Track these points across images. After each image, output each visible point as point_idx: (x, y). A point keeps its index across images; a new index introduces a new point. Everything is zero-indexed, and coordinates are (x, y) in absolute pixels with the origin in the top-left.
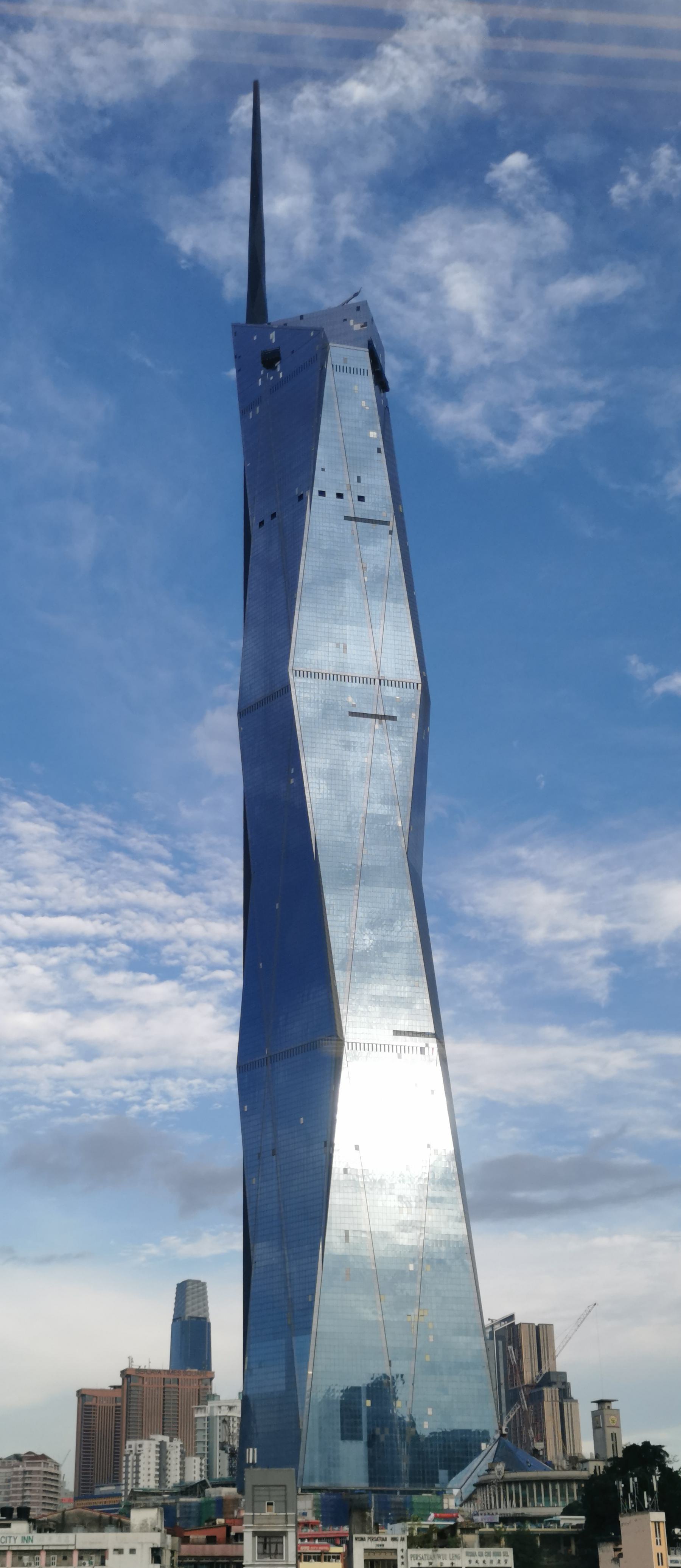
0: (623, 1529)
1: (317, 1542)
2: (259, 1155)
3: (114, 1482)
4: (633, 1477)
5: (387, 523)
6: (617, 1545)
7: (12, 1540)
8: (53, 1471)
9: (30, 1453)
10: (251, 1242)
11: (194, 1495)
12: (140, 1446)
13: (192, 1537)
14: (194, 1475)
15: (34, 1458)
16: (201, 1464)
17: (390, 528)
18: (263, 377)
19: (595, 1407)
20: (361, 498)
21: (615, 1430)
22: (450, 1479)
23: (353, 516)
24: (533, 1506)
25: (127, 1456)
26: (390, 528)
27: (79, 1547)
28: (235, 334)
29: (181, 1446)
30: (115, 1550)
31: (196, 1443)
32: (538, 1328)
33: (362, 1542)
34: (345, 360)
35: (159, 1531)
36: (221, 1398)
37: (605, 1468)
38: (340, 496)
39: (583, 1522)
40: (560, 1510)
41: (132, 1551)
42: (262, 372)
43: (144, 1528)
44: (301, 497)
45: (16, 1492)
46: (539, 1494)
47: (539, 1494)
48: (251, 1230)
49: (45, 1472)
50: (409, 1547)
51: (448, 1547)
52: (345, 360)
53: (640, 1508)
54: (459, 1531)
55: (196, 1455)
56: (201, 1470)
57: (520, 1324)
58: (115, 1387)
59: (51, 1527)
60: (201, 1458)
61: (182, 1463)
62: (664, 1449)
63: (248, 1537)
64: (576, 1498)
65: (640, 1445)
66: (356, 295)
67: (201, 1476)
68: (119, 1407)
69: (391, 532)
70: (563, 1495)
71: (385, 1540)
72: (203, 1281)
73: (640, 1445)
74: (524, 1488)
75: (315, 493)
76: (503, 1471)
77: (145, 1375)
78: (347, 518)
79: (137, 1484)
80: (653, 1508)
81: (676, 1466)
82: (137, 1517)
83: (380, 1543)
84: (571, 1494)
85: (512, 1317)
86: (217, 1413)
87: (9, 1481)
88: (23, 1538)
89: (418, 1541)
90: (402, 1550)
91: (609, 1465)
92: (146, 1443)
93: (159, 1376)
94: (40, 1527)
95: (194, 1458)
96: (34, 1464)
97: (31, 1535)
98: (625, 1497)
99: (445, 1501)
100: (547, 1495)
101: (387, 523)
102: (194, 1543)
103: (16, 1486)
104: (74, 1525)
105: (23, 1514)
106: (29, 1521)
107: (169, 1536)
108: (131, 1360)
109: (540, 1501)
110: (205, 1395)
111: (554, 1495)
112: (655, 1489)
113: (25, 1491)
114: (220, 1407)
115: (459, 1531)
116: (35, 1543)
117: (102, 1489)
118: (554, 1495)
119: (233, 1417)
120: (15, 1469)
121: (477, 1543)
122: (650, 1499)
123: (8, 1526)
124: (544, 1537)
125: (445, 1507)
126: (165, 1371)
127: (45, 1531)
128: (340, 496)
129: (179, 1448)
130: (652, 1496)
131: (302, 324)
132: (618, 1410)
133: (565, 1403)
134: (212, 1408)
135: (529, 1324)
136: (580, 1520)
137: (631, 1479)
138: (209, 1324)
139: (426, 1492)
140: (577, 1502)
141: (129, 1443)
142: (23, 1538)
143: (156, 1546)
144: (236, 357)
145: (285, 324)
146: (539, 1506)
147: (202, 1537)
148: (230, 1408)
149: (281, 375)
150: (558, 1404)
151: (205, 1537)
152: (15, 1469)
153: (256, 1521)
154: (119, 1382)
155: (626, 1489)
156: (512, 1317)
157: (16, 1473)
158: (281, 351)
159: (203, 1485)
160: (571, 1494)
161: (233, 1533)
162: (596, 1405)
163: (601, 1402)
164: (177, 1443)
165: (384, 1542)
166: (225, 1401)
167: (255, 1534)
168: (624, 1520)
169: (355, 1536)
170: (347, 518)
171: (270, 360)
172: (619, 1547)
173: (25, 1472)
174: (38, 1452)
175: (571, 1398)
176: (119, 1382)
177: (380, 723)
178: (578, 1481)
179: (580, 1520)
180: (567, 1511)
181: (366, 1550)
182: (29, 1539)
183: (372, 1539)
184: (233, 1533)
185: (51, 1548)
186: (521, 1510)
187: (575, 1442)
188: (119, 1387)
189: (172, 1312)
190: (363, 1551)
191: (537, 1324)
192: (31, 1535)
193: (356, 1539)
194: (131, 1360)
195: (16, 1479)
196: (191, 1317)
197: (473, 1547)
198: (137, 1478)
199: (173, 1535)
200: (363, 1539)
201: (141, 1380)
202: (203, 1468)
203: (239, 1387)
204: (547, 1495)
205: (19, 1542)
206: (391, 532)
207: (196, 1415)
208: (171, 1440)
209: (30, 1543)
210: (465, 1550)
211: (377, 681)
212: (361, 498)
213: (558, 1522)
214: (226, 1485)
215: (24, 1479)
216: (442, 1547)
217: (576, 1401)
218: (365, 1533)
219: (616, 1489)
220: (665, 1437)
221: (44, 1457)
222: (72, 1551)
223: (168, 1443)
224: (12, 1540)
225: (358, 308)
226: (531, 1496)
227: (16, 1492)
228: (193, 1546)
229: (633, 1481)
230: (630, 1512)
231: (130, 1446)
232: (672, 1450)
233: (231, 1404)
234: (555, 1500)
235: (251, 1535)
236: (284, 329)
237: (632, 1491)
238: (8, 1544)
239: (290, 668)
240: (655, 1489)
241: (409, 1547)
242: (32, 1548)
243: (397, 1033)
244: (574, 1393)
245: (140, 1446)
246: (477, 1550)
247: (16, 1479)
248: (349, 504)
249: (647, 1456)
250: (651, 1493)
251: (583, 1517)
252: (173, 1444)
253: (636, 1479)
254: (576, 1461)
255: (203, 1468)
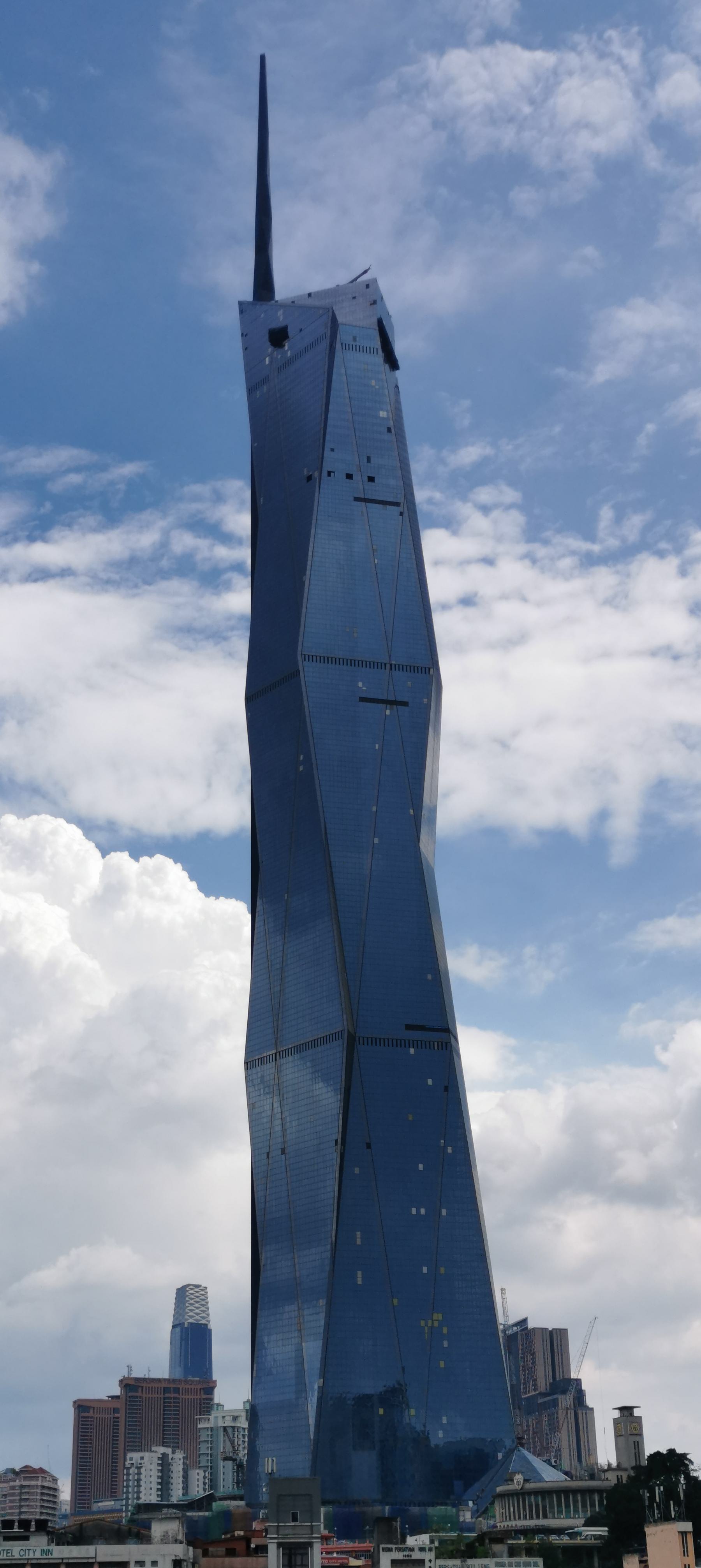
0: (649, 1540)
1: (335, 1555)
2: (268, 1154)
3: (112, 1496)
4: (659, 1486)
5: (397, 504)
6: (643, 1556)
7: (31, 1552)
8: (51, 1485)
9: (26, 1467)
10: (260, 1244)
11: (200, 1509)
12: (142, 1458)
13: (211, 1549)
14: (198, 1491)
15: (28, 1472)
16: (205, 1477)
17: (401, 509)
18: (271, 355)
19: (617, 1414)
20: (371, 479)
21: (637, 1439)
22: (465, 1490)
23: (362, 497)
24: (554, 1518)
25: (128, 1469)
26: (401, 509)
27: (99, 1559)
28: (241, 312)
29: (184, 1458)
30: (136, 1562)
31: (200, 1455)
32: (551, 1332)
33: (389, 1553)
34: (355, 339)
35: (181, 1543)
36: (225, 1408)
37: (629, 1477)
38: (349, 476)
39: (606, 1534)
40: (582, 1521)
41: (154, 1563)
42: (270, 350)
43: (165, 1540)
44: (309, 478)
45: (11, 1508)
46: (559, 1505)
47: (559, 1505)
48: (259, 1232)
49: (43, 1487)
50: (437, 1557)
51: (476, 1558)
52: (355, 339)
53: (666, 1518)
54: (487, 1541)
55: (200, 1467)
56: (205, 1484)
57: (534, 1329)
58: (113, 1397)
59: (69, 1540)
60: (205, 1471)
61: (186, 1477)
62: (688, 1457)
63: (272, 1549)
64: (597, 1509)
65: (665, 1452)
66: (365, 272)
67: (205, 1490)
68: (118, 1418)
69: (402, 514)
70: (584, 1506)
71: (412, 1550)
72: (203, 1285)
73: (665, 1452)
74: (543, 1499)
75: (325, 473)
76: (522, 1481)
77: (144, 1385)
78: (357, 499)
79: (138, 1498)
80: (680, 1518)
81: (698, 1474)
82: (157, 1529)
83: (407, 1553)
84: (593, 1505)
85: (525, 1321)
86: (221, 1424)
87: (5, 1496)
88: (43, 1551)
89: (444, 1551)
90: (430, 1561)
91: (632, 1473)
92: (146, 1455)
93: (159, 1385)
94: (60, 1538)
95: (197, 1471)
96: (31, 1478)
97: (50, 1548)
98: (651, 1507)
99: (461, 1513)
100: (567, 1506)
101: (397, 504)
102: (213, 1556)
103: (11, 1501)
104: (94, 1537)
105: (42, 1526)
106: (48, 1533)
107: (191, 1548)
108: (130, 1368)
109: (560, 1512)
110: (206, 1405)
111: (575, 1506)
112: (682, 1498)
113: (21, 1506)
114: (224, 1417)
115: (487, 1541)
116: (55, 1555)
117: (100, 1504)
118: (575, 1506)
119: (238, 1428)
120: (12, 1484)
121: (506, 1554)
122: (677, 1509)
123: (26, 1538)
124: (566, 1549)
125: (461, 1519)
126: (165, 1380)
127: (63, 1545)
128: (349, 476)
129: (182, 1461)
130: (679, 1507)
131: (309, 302)
132: (640, 1417)
133: (580, 1412)
134: (216, 1418)
135: (542, 1329)
136: (602, 1531)
137: (657, 1488)
138: (210, 1330)
139: (442, 1504)
140: (599, 1513)
141: (129, 1455)
142: (43, 1551)
143: (178, 1558)
144: (242, 335)
145: (293, 302)
146: (559, 1518)
147: (222, 1550)
148: (235, 1418)
149: (289, 354)
150: (573, 1412)
151: (224, 1549)
152: (12, 1484)
153: (281, 1532)
154: (117, 1391)
155: (652, 1498)
156: (525, 1321)
157: (13, 1488)
158: (289, 330)
159: (210, 1499)
160: (593, 1505)
161: (253, 1546)
162: (618, 1412)
163: (622, 1409)
164: (179, 1455)
165: (411, 1553)
166: (231, 1411)
167: (279, 1545)
168: (649, 1530)
169: (382, 1546)
170: (357, 499)
171: (278, 337)
172: (645, 1558)
173: (22, 1487)
174: (36, 1466)
175: (587, 1407)
176: (117, 1391)
177: (391, 709)
178: (600, 1491)
179: (602, 1531)
180: (589, 1523)
181: (394, 1562)
182: (49, 1552)
183: (399, 1550)
184: (253, 1546)
185: (71, 1561)
186: (542, 1522)
187: (592, 1451)
188: (117, 1397)
189: (172, 1319)
190: (389, 1562)
191: (550, 1329)
192: (50, 1548)
193: (384, 1549)
194: (130, 1368)
195: (13, 1495)
196: (191, 1324)
197: (501, 1556)
198: (139, 1492)
199: (195, 1547)
200: (390, 1550)
201: (140, 1390)
202: (207, 1481)
203: (247, 1395)
204: (567, 1506)
205: (38, 1555)
206: (402, 514)
207: (199, 1426)
208: (173, 1452)
209: (50, 1556)
210: (495, 1560)
211: (388, 666)
212: (371, 479)
213: (580, 1534)
214: (233, 1498)
215: (21, 1494)
216: (471, 1557)
217: (592, 1409)
218: (391, 1543)
219: (641, 1498)
220: (687, 1444)
221: (42, 1470)
222: (93, 1563)
223: (170, 1457)
224: (31, 1552)
225: (368, 286)
226: (552, 1507)
227: (11, 1508)
228: (212, 1559)
229: (658, 1490)
230: (655, 1522)
231: (131, 1459)
232: (694, 1457)
233: (236, 1414)
234: (576, 1511)
235: (275, 1546)
236: (292, 305)
237: (658, 1500)
238: (27, 1557)
239: (299, 653)
240: (682, 1498)
241: (437, 1557)
242: (51, 1561)
243: (409, 1027)
244: (590, 1402)
245: (142, 1458)
246: (506, 1560)
247: (13, 1495)
248: (359, 485)
249: (672, 1462)
250: (678, 1503)
251: (606, 1529)
252: (175, 1456)
253: (662, 1488)
254: (594, 1473)
255: (207, 1481)
